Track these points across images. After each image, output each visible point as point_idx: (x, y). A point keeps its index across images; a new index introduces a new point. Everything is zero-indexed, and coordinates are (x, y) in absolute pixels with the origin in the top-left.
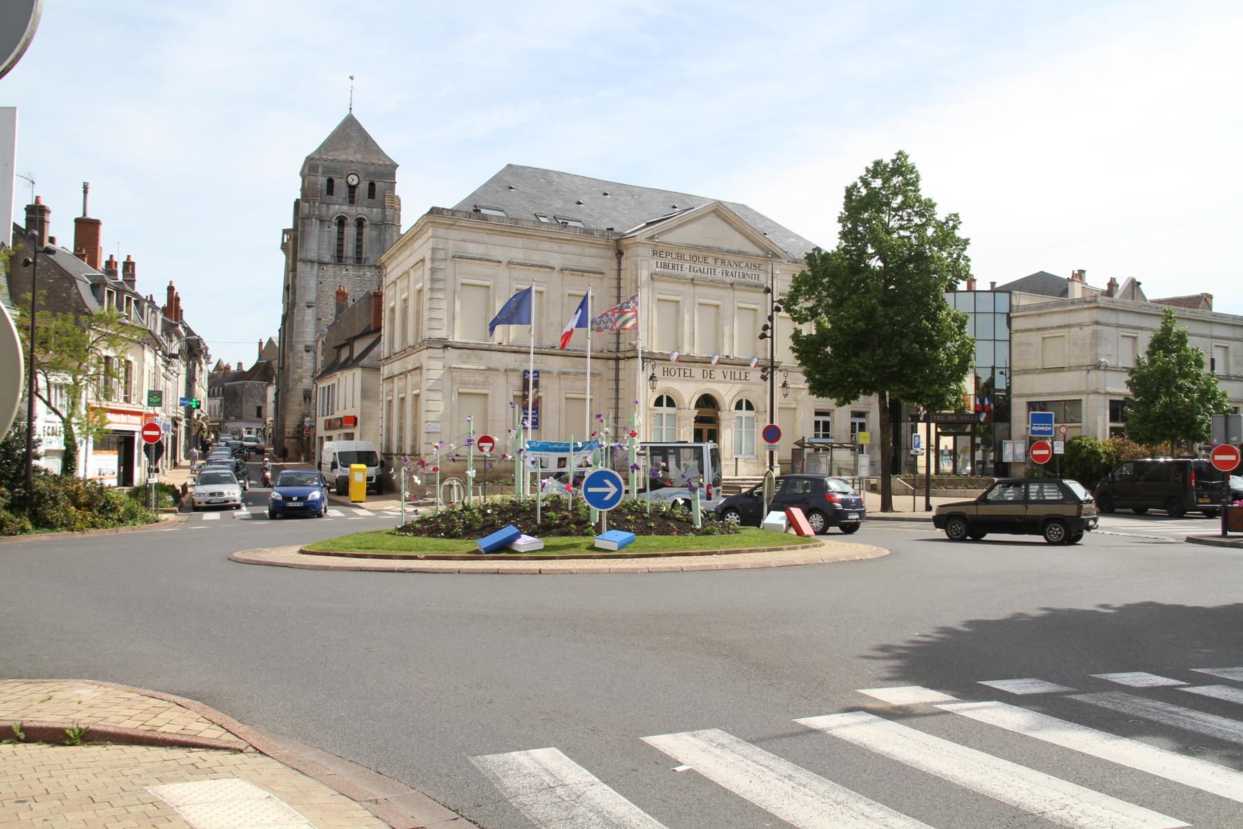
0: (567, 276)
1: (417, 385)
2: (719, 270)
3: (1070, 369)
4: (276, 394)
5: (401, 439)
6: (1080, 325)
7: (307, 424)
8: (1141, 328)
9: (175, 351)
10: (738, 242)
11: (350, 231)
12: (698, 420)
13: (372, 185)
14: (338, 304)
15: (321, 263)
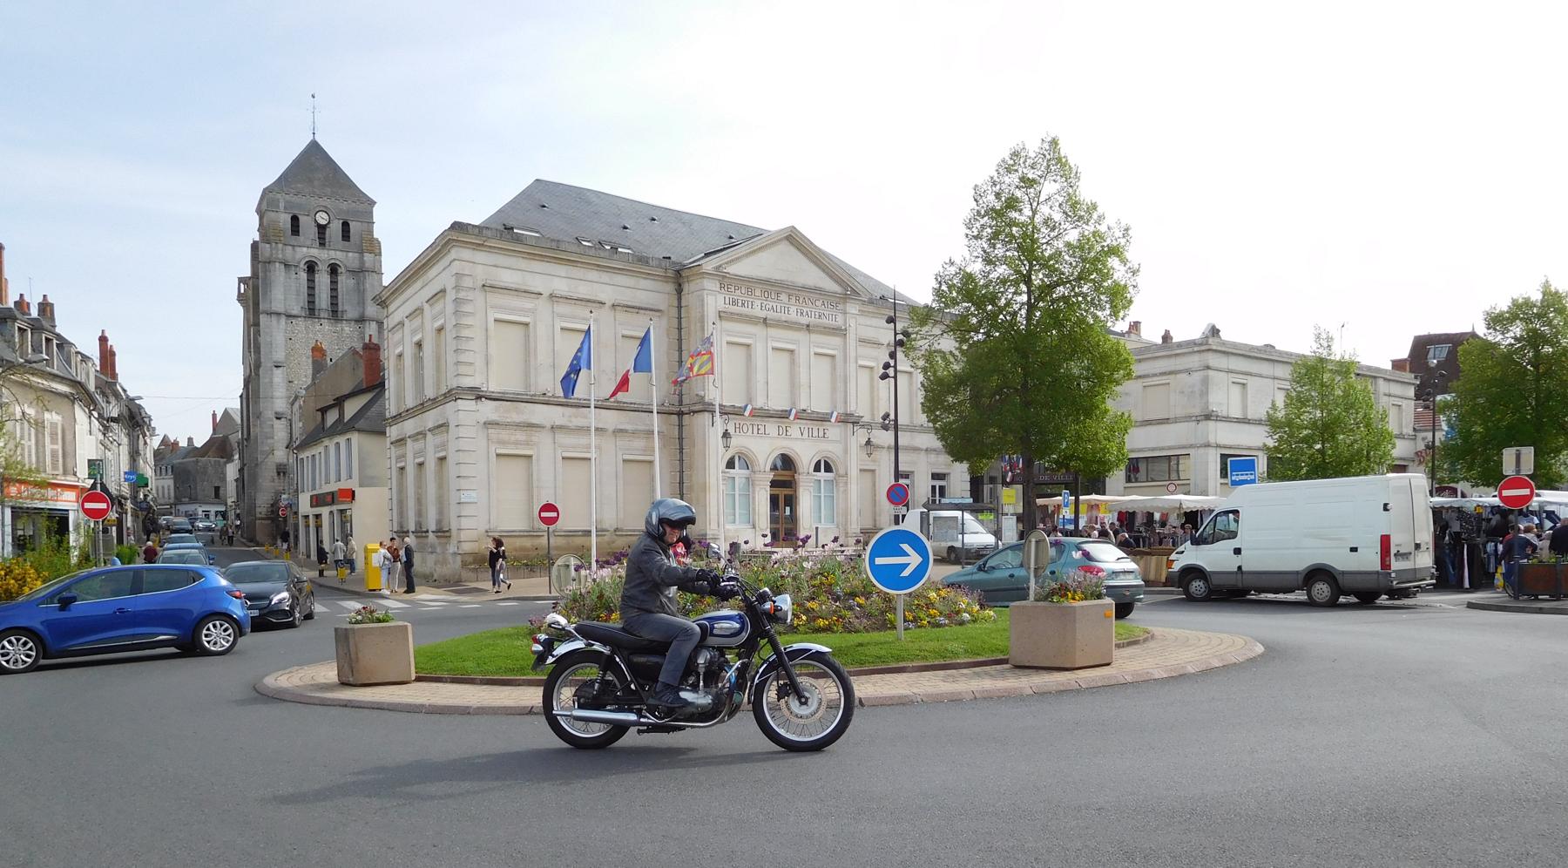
0: (621, 316)
1: (444, 446)
2: (793, 309)
3: (1176, 420)
4: (241, 470)
5: (419, 513)
6: (1189, 371)
7: (283, 503)
8: (1250, 374)
10: (812, 276)
11: (323, 279)
12: (774, 484)
13: (346, 225)
14: (314, 362)
15: (289, 316)
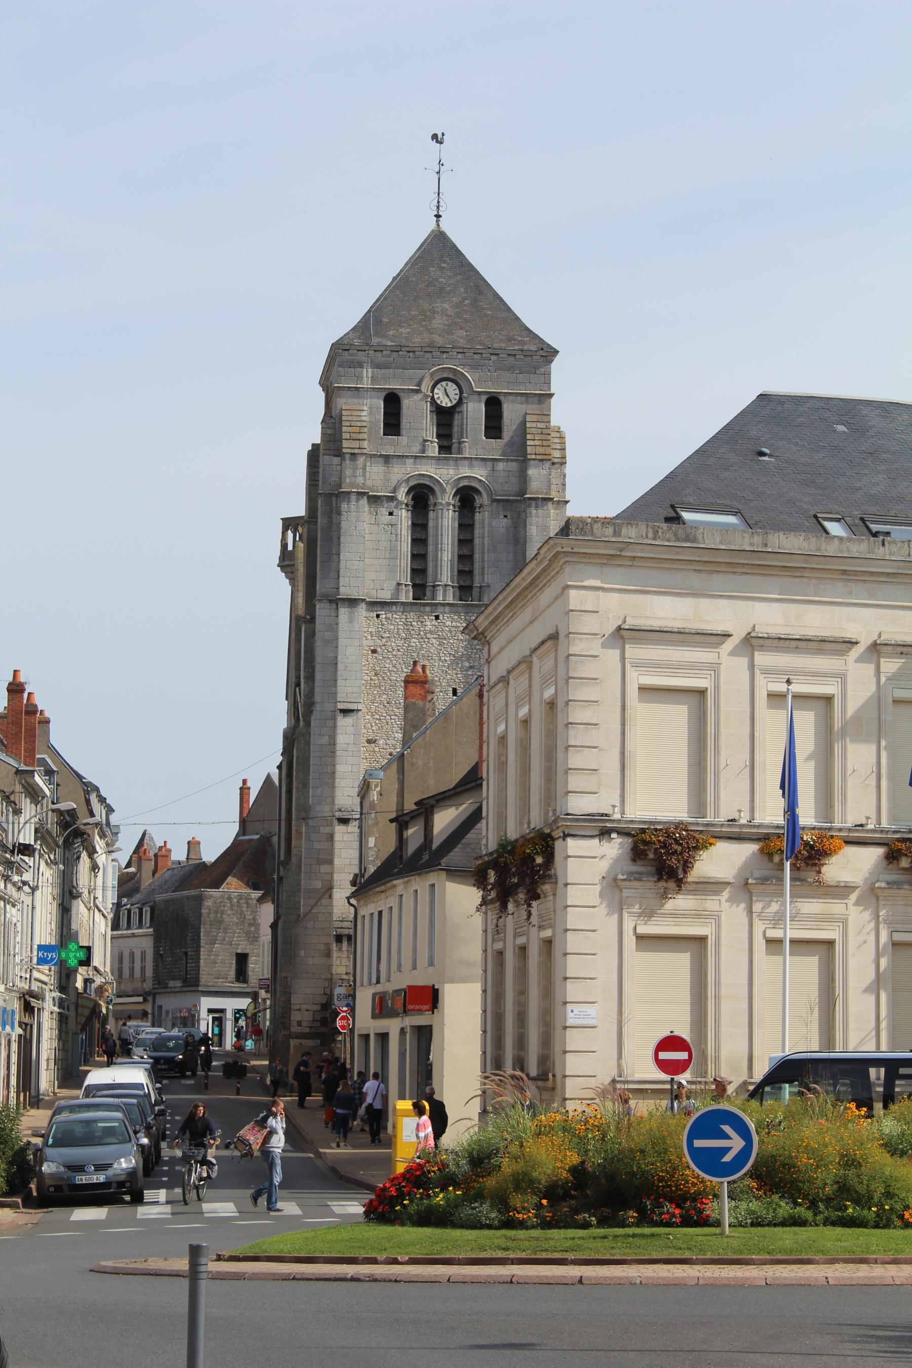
4: (274, 926)
9: (27, 837)
11: (446, 521)
13: (494, 404)
